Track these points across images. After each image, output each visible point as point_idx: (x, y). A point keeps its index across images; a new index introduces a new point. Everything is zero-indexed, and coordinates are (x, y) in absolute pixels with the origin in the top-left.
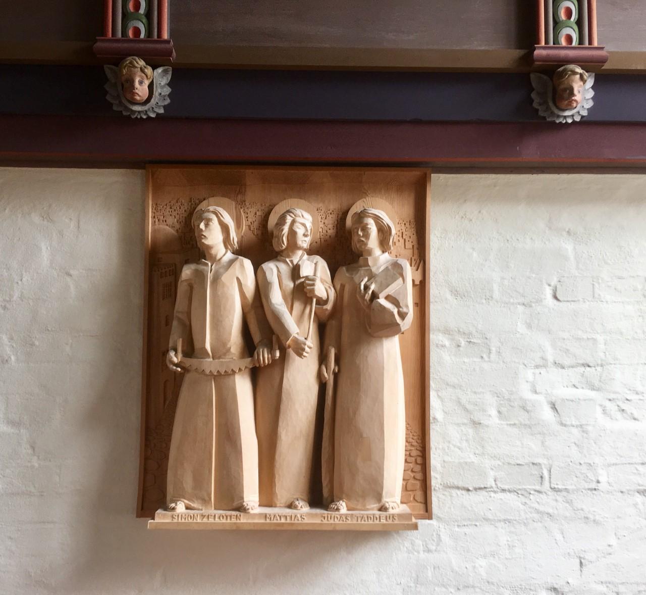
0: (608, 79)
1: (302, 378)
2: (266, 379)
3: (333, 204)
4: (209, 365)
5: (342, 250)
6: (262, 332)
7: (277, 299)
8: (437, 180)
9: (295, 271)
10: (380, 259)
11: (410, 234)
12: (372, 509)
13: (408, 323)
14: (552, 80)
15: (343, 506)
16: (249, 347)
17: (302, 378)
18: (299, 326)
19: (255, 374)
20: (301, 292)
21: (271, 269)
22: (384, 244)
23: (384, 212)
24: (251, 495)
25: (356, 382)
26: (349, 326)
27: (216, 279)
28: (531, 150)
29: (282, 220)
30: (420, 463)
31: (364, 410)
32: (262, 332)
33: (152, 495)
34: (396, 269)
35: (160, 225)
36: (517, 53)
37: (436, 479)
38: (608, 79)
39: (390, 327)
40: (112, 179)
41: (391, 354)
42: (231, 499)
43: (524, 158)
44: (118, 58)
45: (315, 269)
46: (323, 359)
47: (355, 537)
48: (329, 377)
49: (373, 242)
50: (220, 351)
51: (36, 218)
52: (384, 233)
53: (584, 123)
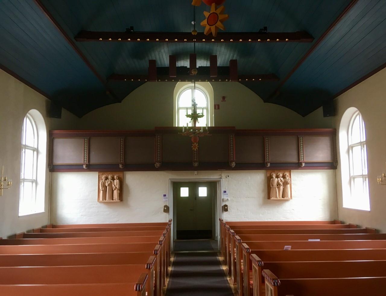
0: (305, 163)
1: (282, 188)
2: (279, 188)
3: (283, 173)
4: (274, 187)
5: (284, 177)
6: (278, 184)
7: (279, 182)
8: (292, 170)
9: (281, 179)
10: (287, 178)
11: (289, 176)
12: (288, 198)
13: (290, 184)
14: (301, 164)
15: (285, 198)
16: (277, 186)
17: (282, 188)
18: (282, 184)
19: (278, 188)
20: (281, 181)
21: (278, 179)
22: (288, 177)
23: (287, 174)
24: (278, 197)
25: (286, 187)
26: (285, 184)
27: (275, 180)
28: (299, 168)
29: (279, 175)
30: (194, 84)
31: (287, 190)
32: (278, 184)
33: (269, 198)
34: (289, 179)
35: (268, 175)
36: (298, 161)
37: (292, 196)
38: (305, 163)
39: (289, 184)
40: (263, 171)
41: (289, 186)
42: (276, 197)
43: (196, 159)
44: (267, 163)
45: (282, 179)
46: (283, 186)
47: (287, 200)
48: (284, 187)
49: (287, 177)
50: (275, 186)
51: (257, 174)
52: (288, 176)
53: (269, 167)
